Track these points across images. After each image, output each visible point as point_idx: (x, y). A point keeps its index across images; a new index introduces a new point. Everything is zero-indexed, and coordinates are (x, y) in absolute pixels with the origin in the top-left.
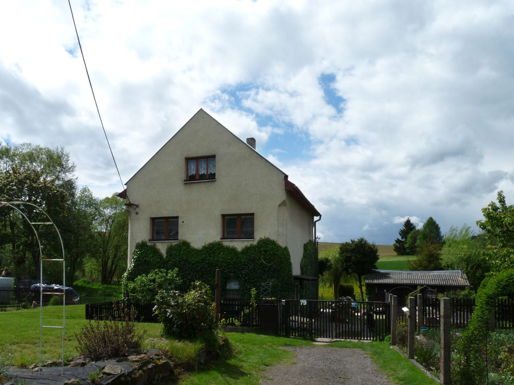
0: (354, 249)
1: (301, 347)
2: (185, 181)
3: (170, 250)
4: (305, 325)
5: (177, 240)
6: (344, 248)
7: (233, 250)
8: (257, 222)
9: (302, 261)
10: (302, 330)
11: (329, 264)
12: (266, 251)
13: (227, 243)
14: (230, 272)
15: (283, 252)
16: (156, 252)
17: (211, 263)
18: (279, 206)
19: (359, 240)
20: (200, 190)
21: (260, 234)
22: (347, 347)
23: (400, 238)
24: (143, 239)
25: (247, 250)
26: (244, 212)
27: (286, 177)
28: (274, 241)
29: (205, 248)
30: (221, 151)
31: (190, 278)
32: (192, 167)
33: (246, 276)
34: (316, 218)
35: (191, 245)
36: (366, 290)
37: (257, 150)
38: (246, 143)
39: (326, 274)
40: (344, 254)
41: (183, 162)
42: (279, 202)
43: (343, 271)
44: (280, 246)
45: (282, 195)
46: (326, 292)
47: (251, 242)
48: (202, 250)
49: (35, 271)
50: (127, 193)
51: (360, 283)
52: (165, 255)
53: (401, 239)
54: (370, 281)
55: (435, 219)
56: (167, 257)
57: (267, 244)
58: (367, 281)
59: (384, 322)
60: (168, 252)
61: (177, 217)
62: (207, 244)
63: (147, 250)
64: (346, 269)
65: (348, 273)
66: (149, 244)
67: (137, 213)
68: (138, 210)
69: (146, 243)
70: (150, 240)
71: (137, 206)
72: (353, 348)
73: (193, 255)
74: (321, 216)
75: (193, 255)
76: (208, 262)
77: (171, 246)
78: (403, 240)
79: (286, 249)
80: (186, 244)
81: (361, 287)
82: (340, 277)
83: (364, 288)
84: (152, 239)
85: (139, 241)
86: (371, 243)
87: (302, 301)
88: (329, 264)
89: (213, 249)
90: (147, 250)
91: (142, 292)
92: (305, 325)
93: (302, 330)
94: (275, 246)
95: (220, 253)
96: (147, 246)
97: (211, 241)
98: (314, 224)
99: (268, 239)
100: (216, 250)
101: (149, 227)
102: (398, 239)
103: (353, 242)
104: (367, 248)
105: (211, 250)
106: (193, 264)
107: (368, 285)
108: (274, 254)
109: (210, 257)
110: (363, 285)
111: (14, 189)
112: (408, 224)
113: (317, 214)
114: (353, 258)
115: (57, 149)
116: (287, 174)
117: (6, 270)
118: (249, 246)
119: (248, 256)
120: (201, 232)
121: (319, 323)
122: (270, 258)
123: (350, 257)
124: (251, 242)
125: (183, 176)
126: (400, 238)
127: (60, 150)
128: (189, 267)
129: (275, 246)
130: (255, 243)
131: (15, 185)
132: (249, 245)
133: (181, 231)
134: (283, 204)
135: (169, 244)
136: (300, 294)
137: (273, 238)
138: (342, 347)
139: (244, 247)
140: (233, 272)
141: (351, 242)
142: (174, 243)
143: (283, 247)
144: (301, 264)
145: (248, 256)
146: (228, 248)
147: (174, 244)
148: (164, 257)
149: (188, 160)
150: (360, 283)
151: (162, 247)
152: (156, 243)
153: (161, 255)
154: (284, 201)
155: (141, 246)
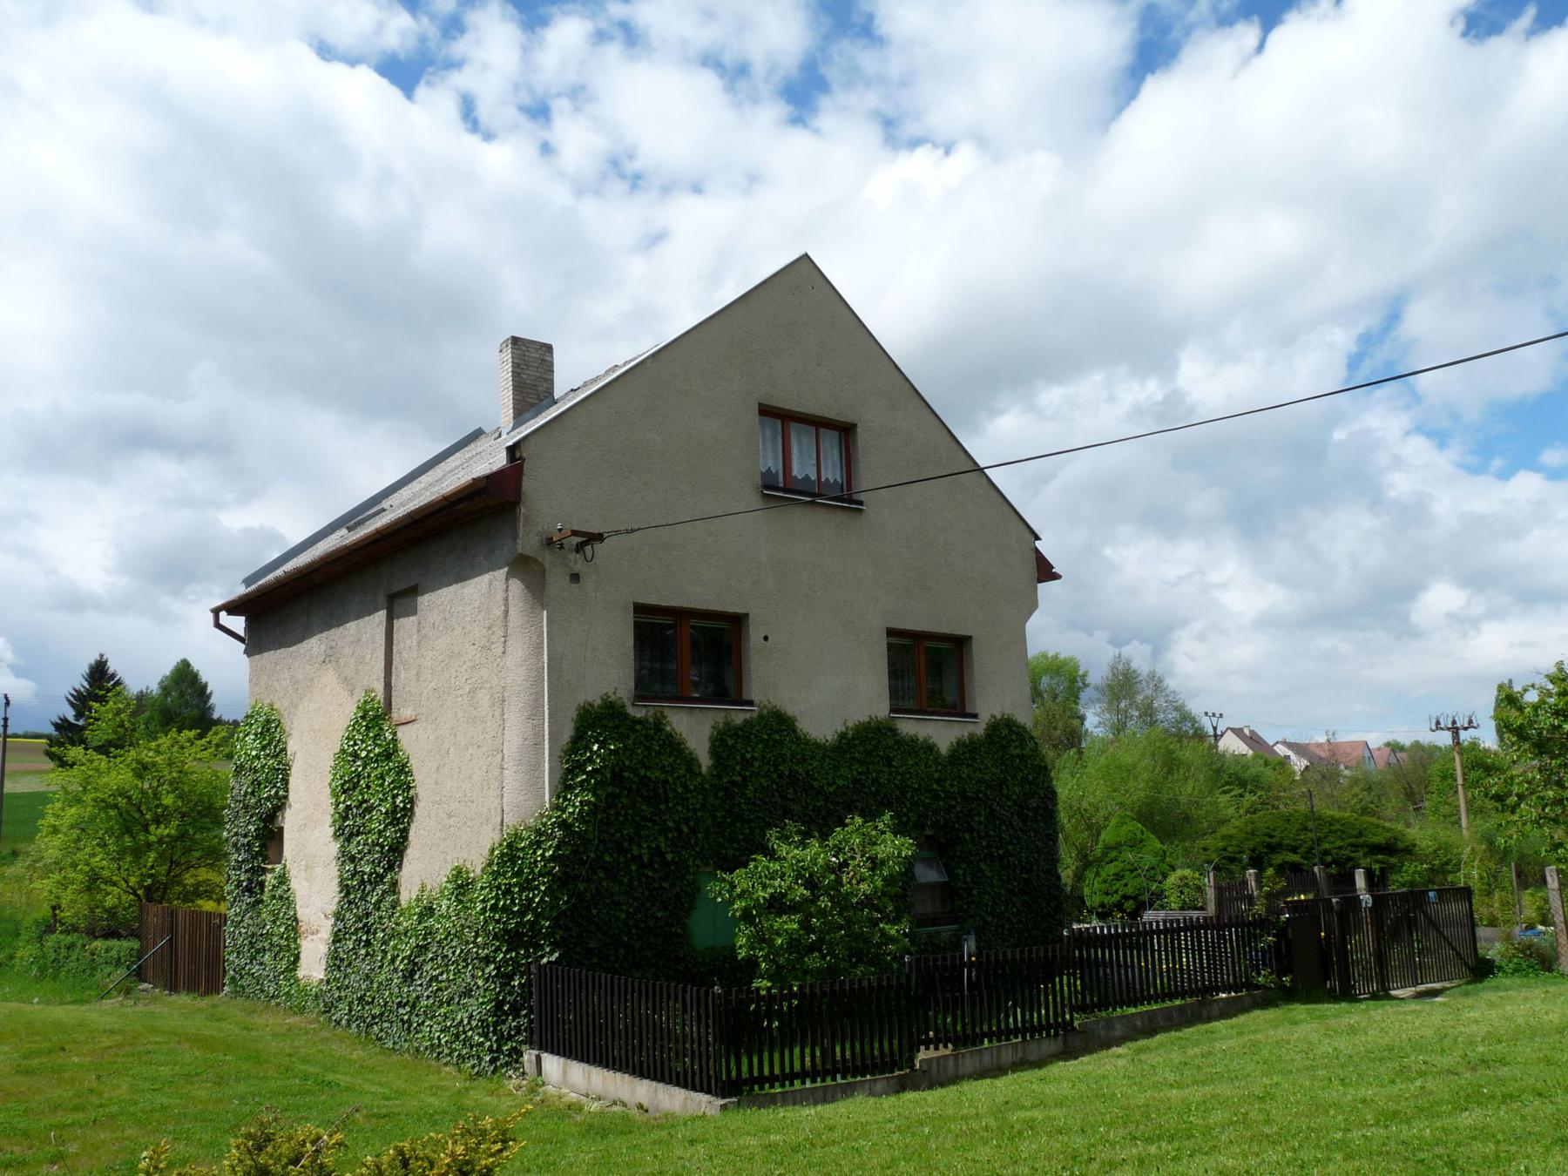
1: (1477, 993)
3: (722, 742)
5: (751, 703)
20: (809, 535)
23: (70, 714)
30: (871, 419)
52: (705, 762)
53: (72, 720)
55: (196, 665)
60: (715, 753)
62: (850, 724)
66: (637, 713)
69: (623, 706)
78: (81, 723)
80: (780, 722)
84: (643, 692)
89: (868, 741)
96: (626, 716)
102: (64, 720)
112: (99, 673)
126: (70, 714)
130: (980, 729)
135: (720, 718)
142: (739, 716)
148: (704, 770)
151: (695, 729)
152: (667, 712)
153: (691, 762)
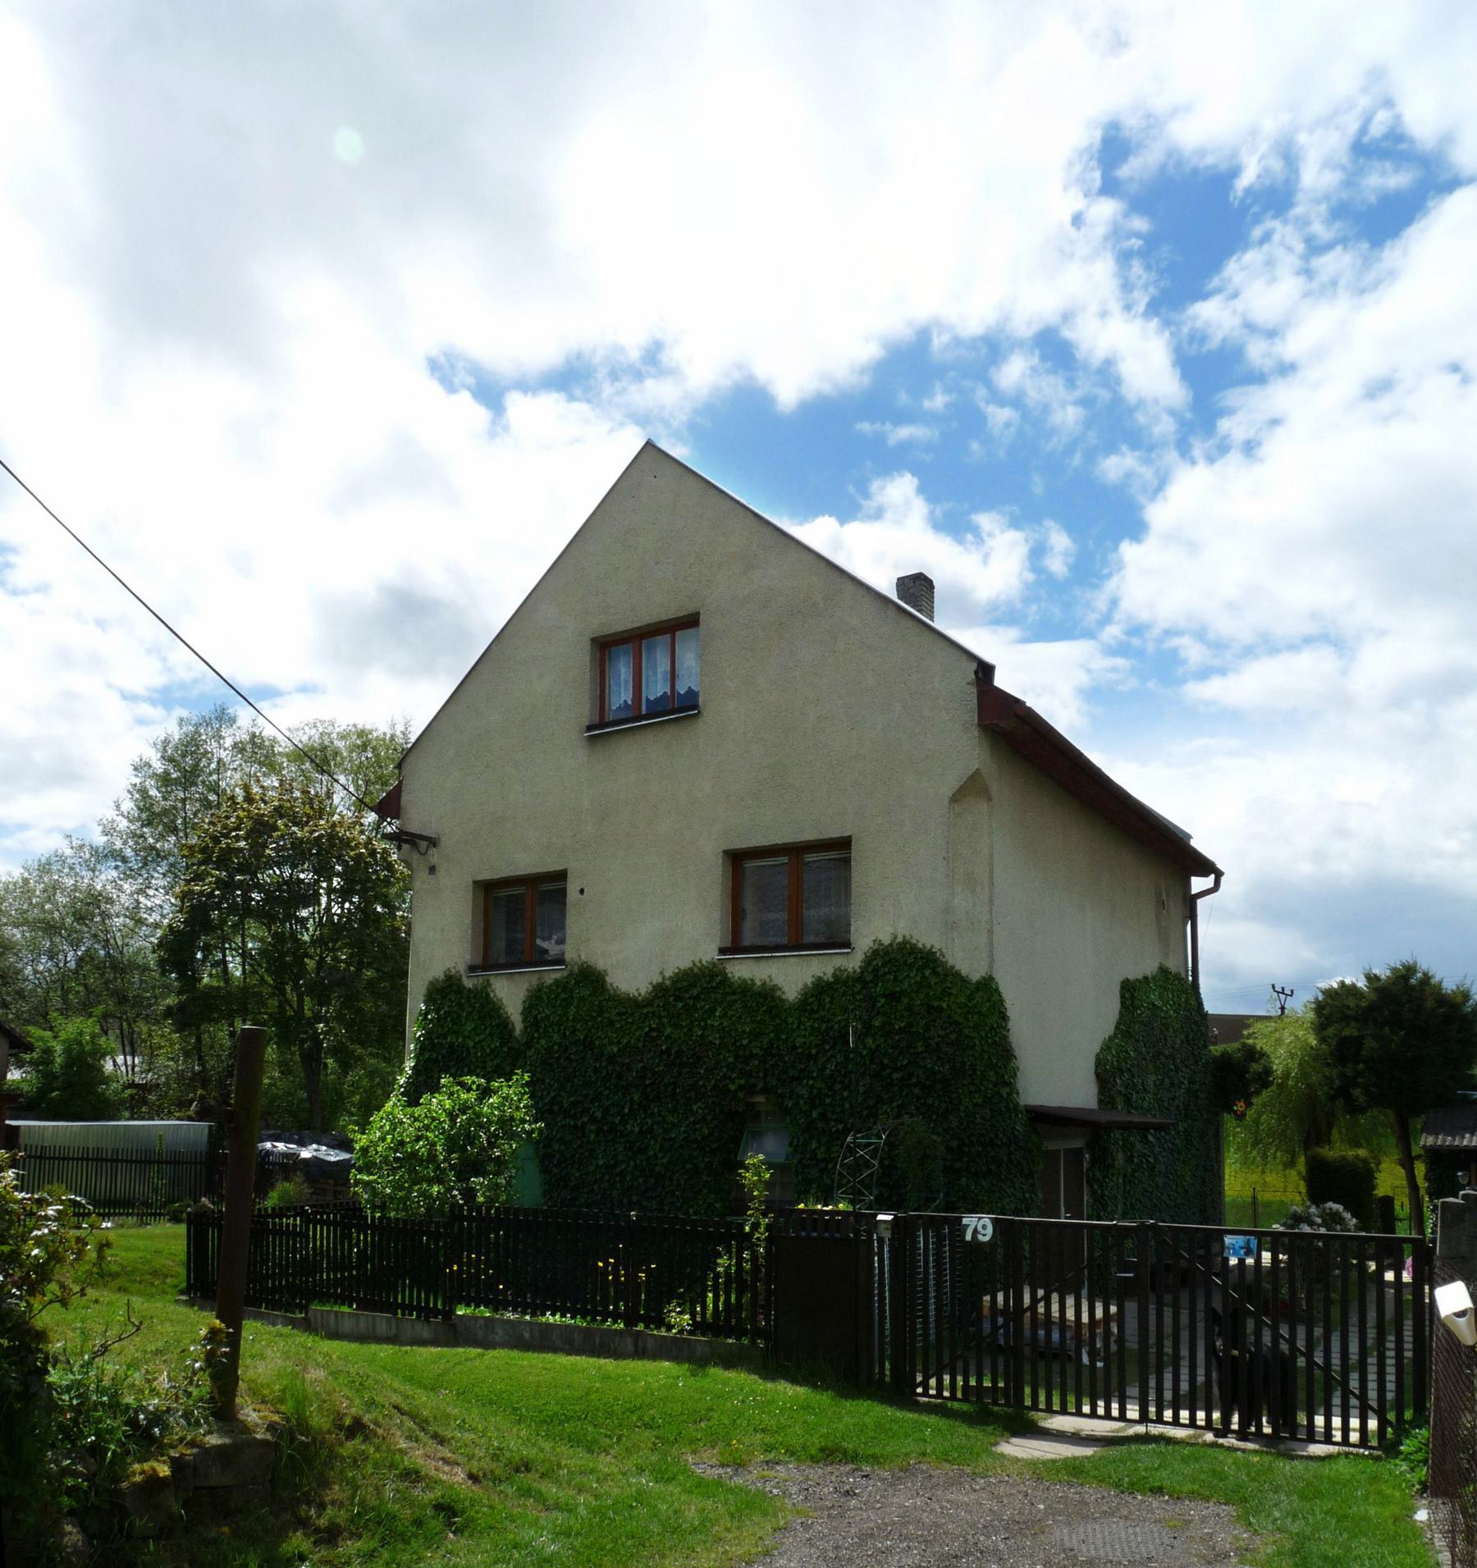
0: (1372, 1007)
2: (589, 728)
3: (535, 1001)
4: (1056, 1336)
6: (1335, 1007)
7: (766, 998)
8: (865, 872)
9: (1106, 1047)
10: (1042, 1355)
11: (1255, 1067)
12: (893, 997)
13: (743, 970)
14: (751, 1090)
15: (970, 998)
16: (488, 1009)
17: (679, 1053)
18: (955, 798)
19: (1394, 970)
20: (643, 760)
21: (875, 924)
22: (1158, 1491)
24: (449, 964)
25: (820, 990)
26: (810, 835)
27: (985, 671)
28: (931, 953)
29: (659, 990)
31: (599, 1114)
32: (623, 670)
33: (813, 1106)
34: (1198, 884)
35: (608, 979)
36: (1426, 1178)
37: (938, 624)
38: (894, 596)
39: (1261, 1108)
40: (1330, 1031)
41: (581, 660)
42: (951, 782)
43: (1333, 1098)
44: (958, 975)
45: (964, 750)
46: (1256, 1180)
47: (839, 962)
48: (647, 1002)
49: (307, 1105)
50: (404, 798)
51: (1406, 1149)
54: (1444, 1140)
56: (525, 1030)
57: (906, 967)
58: (1430, 1140)
59: (1301, 1396)
61: (561, 876)
62: (668, 973)
63: (460, 1005)
64: (1343, 1092)
65: (1354, 1109)
67: (432, 870)
68: (434, 856)
69: (460, 979)
70: (472, 968)
71: (433, 842)
72: (1193, 1495)
73: (611, 1023)
74: (1219, 875)
75: (611, 1023)
76: (668, 1051)
77: (539, 989)
79: (988, 986)
80: (590, 978)
81: (1407, 1163)
82: (1330, 1126)
83: (1420, 1169)
85: (437, 972)
86: (1449, 985)
87: (971, 1221)
88: (1255, 1067)
89: (693, 991)
90: (460, 1005)
91: (393, 1165)
92: (1056, 1336)
93: (1042, 1355)
94: (935, 973)
95: (713, 1010)
97: (685, 963)
98: (1189, 907)
99: (905, 942)
100: (697, 998)
101: (468, 919)
103: (1371, 978)
104: (1430, 1003)
105: (679, 998)
106: (611, 1059)
107: (1435, 1156)
108: (930, 1009)
109: (676, 1026)
110: (1418, 1157)
111: (241, 850)
113: (1205, 867)
114: (1370, 1043)
115: (393, 726)
116: (987, 656)
117: (202, 1097)
118: (829, 977)
119: (822, 1020)
120: (646, 931)
121: (1168, 1313)
122: (910, 1025)
123: (1358, 1041)
124: (839, 962)
125: (584, 712)
127: (399, 728)
128: (596, 1071)
129: (935, 973)
130: (853, 962)
131: (246, 839)
132: (830, 971)
133: (575, 923)
134: (971, 788)
135: (534, 981)
136: (1093, 1192)
137: (928, 938)
138: (1133, 1488)
139: (809, 981)
140: (765, 1090)
141: (1362, 983)
142: (552, 975)
143: (975, 977)
144: (1099, 1062)
145: (822, 1020)
146: (745, 990)
147: (549, 980)
148: (517, 1032)
149: (605, 647)
150: (1406, 1149)
151: (510, 994)
152: (492, 980)
153: (505, 1025)
154: (975, 777)
155: (444, 992)
